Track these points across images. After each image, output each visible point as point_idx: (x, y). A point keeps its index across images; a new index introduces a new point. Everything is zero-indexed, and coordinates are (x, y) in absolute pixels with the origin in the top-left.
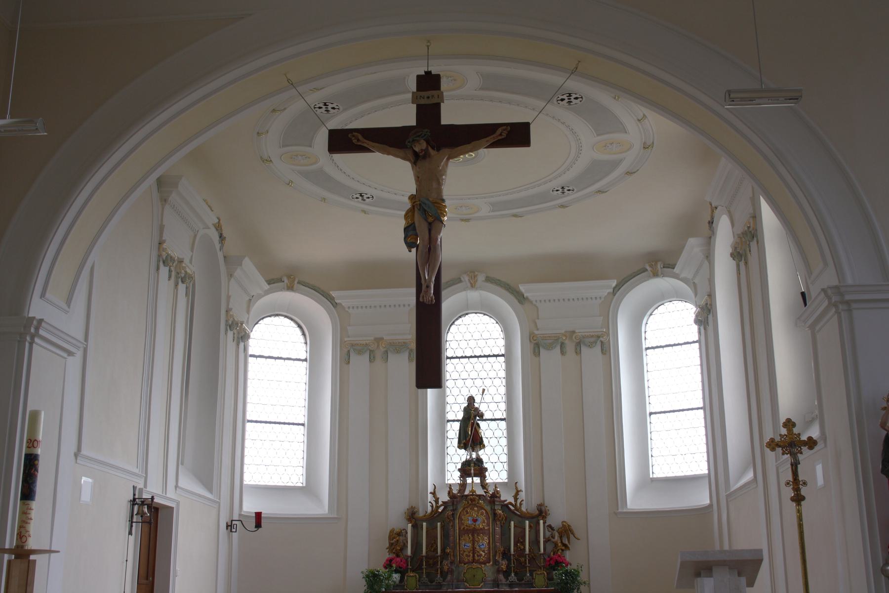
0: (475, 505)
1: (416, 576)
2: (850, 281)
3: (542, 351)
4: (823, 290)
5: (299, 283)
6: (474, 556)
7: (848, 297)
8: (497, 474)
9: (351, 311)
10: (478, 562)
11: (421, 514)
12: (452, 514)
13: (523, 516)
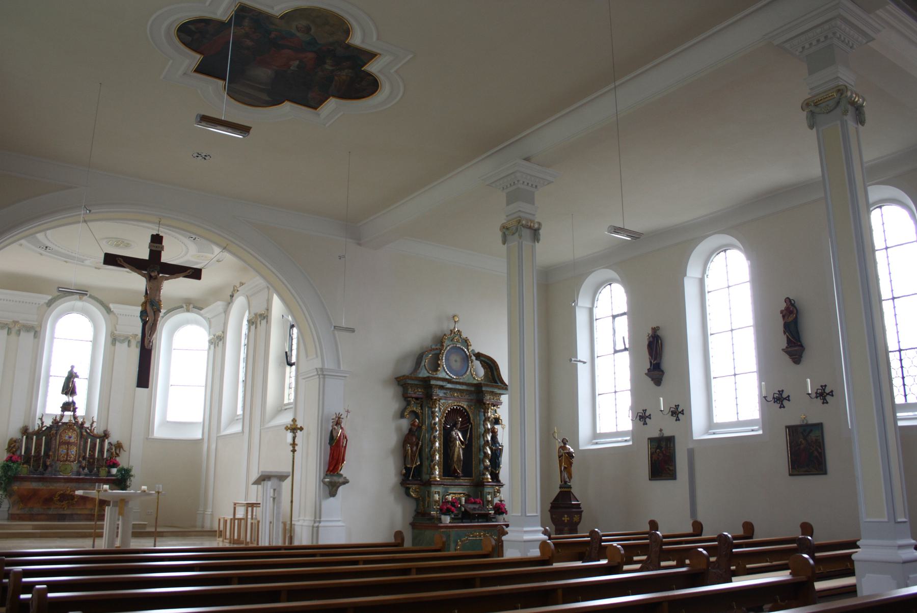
0: (71, 429)
1: (27, 467)
2: (326, 367)
3: (117, 343)
4: (316, 369)
6: (67, 458)
7: (325, 373)
8: (81, 412)
10: (69, 461)
11: (31, 430)
12: (56, 433)
13: (95, 437)
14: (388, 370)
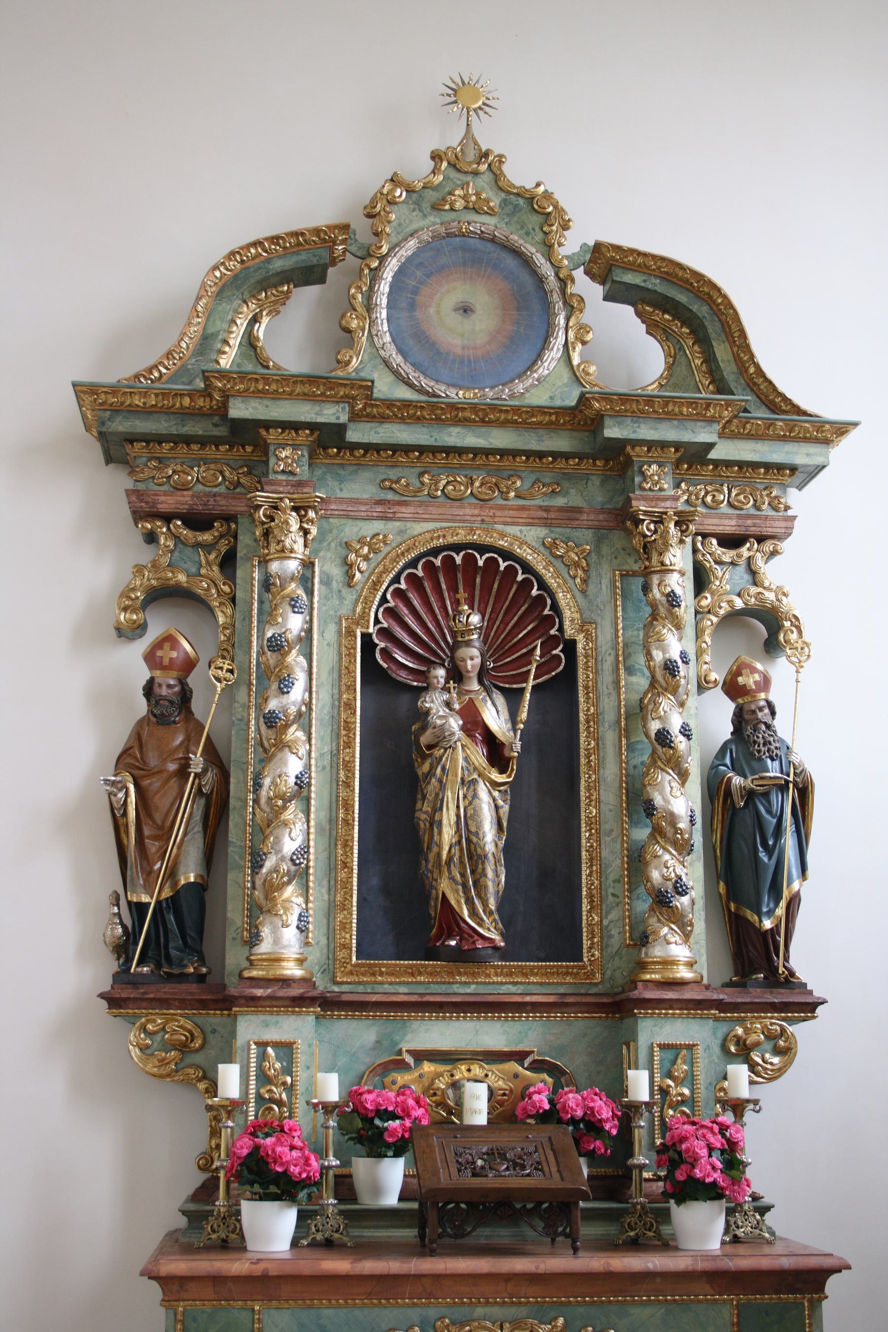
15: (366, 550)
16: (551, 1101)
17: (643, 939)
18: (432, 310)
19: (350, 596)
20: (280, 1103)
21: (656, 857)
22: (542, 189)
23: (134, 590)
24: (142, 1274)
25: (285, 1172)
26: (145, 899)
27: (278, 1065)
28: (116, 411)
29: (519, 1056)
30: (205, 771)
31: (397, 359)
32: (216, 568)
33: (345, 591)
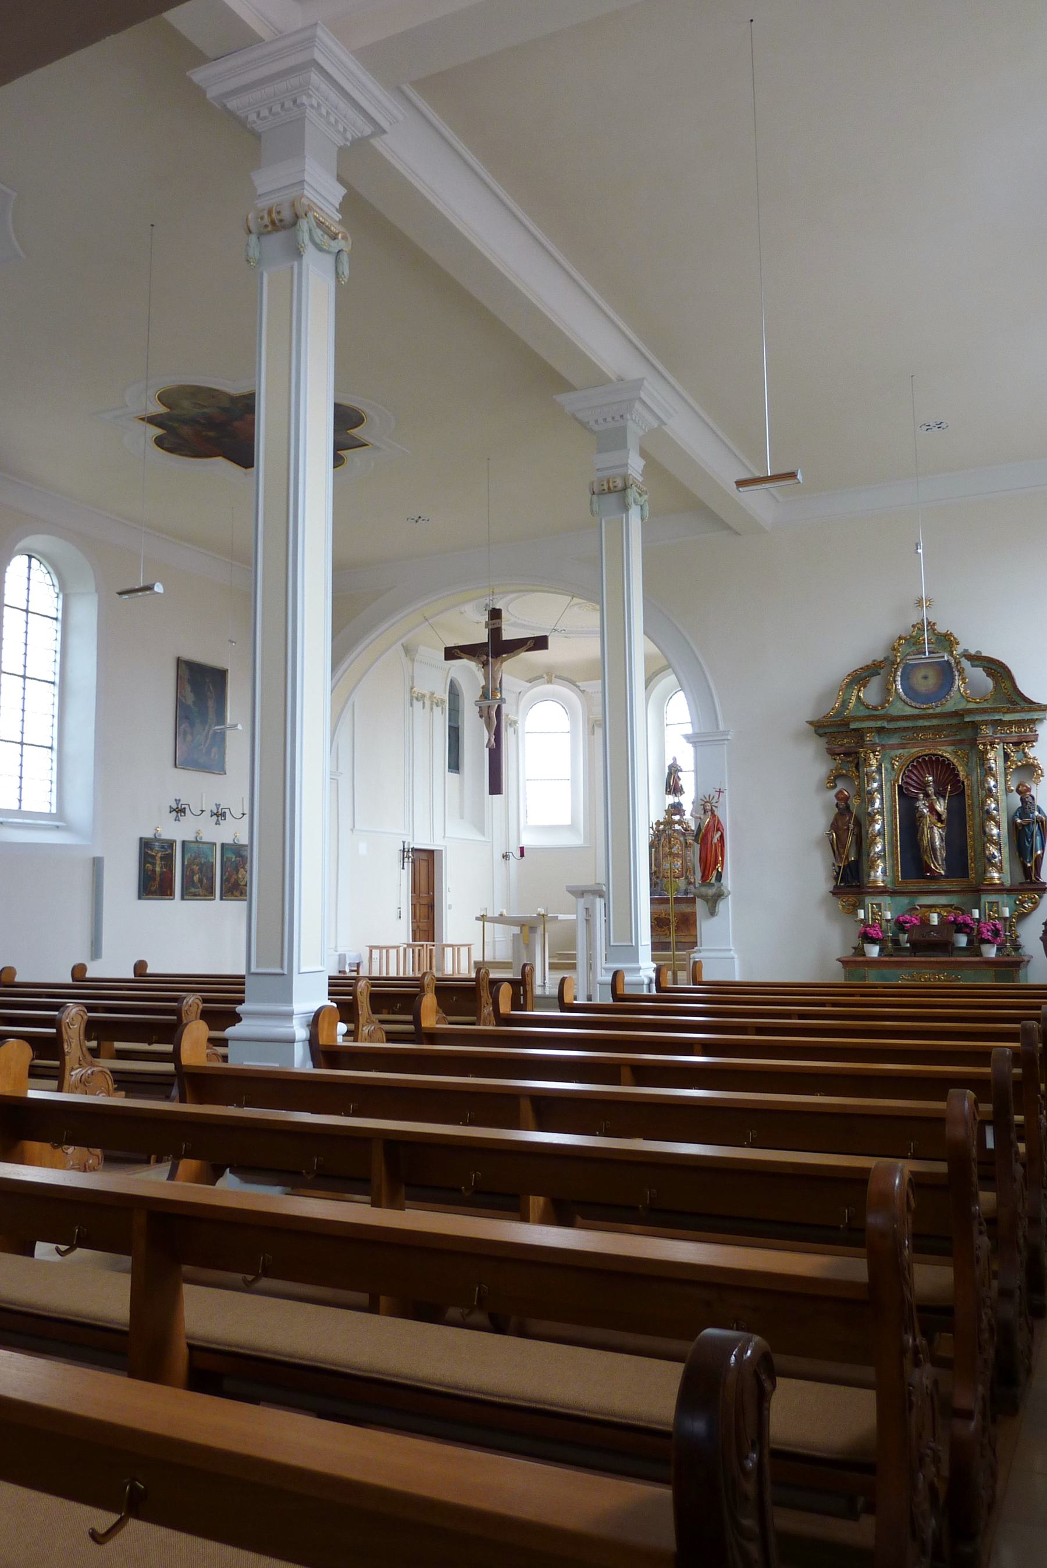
5: (555, 677)
9: (593, 695)
12: (658, 843)
14: (807, 712)
15: (898, 759)
16: (955, 918)
17: (985, 872)
18: (915, 679)
19: (894, 773)
20: (878, 920)
21: (988, 847)
22: (949, 633)
23: (830, 777)
24: (837, 960)
25: (872, 936)
26: (841, 865)
27: (877, 910)
28: (819, 727)
29: (951, 906)
30: (854, 828)
31: (904, 697)
32: (854, 768)
33: (892, 772)
